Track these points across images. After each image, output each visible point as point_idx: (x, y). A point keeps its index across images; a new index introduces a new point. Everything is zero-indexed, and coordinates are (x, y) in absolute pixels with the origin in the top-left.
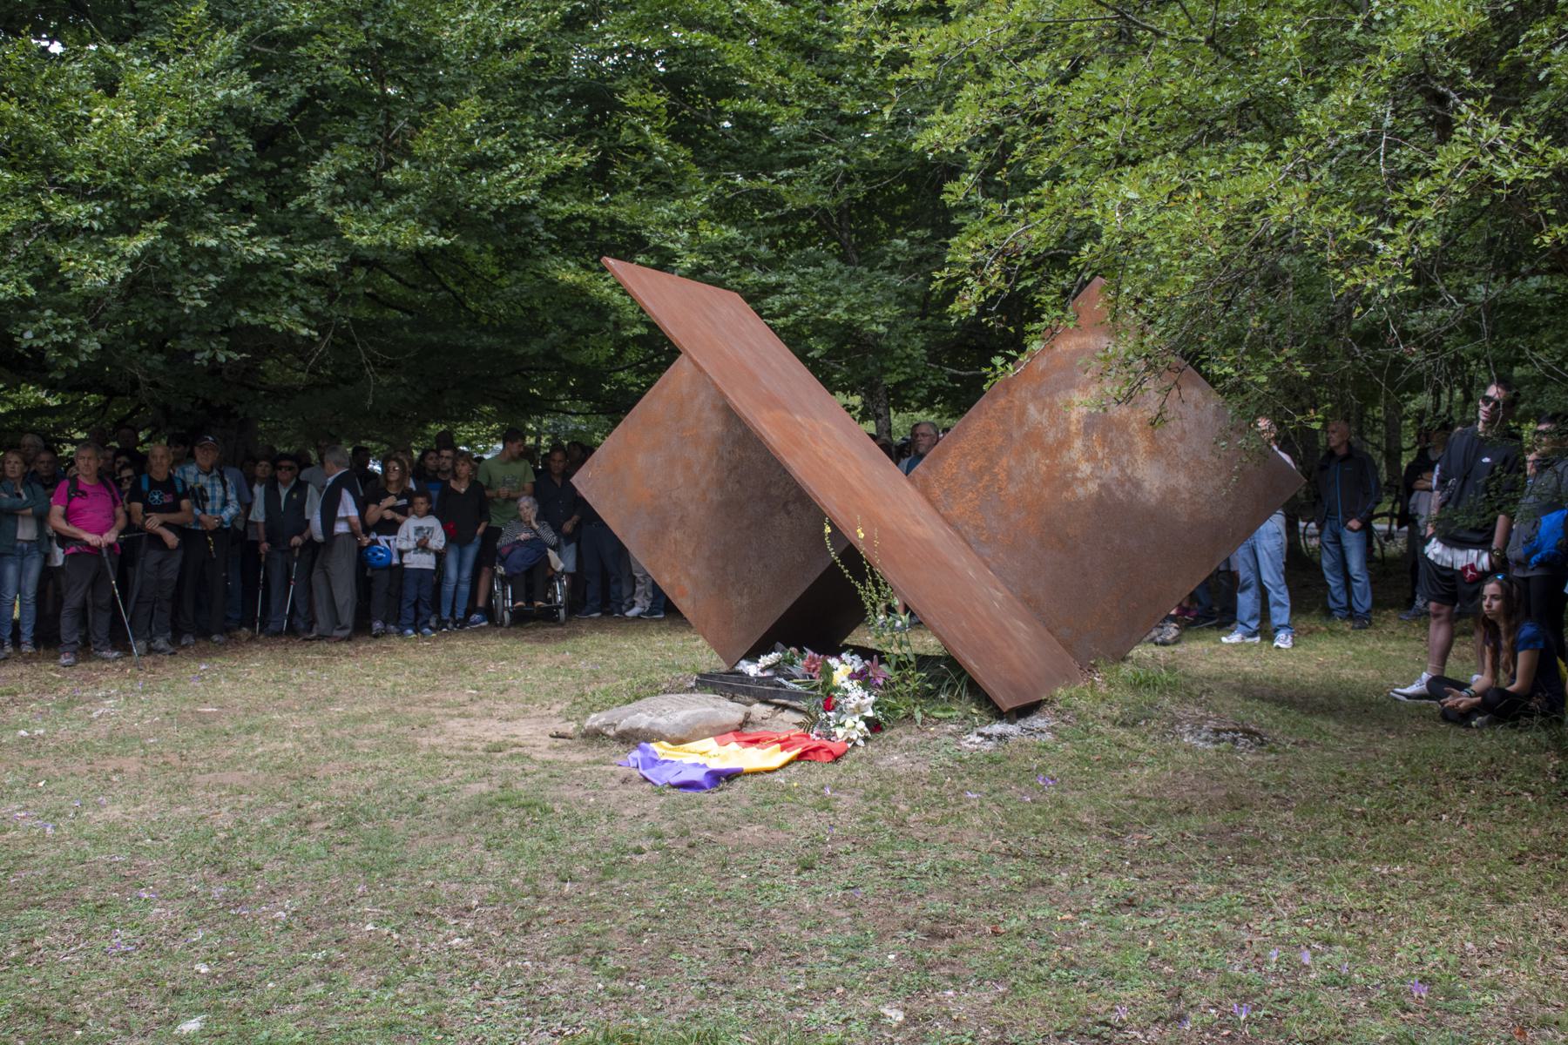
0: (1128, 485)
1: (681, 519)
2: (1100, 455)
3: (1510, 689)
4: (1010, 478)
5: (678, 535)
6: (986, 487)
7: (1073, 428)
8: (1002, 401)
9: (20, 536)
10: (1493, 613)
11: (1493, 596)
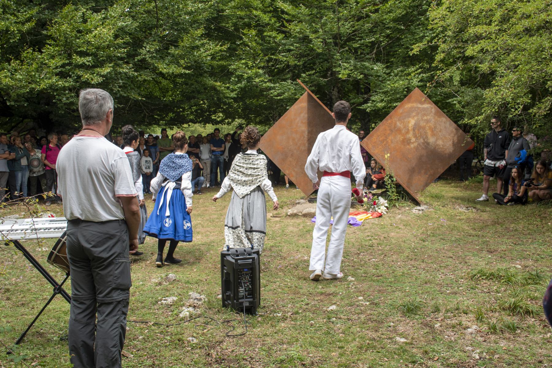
0: (425, 144)
1: (292, 155)
2: (418, 136)
3: (518, 195)
4: (392, 142)
5: (291, 159)
6: (385, 145)
7: (410, 129)
8: (389, 121)
9: (22, 164)
10: (515, 177)
11: (515, 172)
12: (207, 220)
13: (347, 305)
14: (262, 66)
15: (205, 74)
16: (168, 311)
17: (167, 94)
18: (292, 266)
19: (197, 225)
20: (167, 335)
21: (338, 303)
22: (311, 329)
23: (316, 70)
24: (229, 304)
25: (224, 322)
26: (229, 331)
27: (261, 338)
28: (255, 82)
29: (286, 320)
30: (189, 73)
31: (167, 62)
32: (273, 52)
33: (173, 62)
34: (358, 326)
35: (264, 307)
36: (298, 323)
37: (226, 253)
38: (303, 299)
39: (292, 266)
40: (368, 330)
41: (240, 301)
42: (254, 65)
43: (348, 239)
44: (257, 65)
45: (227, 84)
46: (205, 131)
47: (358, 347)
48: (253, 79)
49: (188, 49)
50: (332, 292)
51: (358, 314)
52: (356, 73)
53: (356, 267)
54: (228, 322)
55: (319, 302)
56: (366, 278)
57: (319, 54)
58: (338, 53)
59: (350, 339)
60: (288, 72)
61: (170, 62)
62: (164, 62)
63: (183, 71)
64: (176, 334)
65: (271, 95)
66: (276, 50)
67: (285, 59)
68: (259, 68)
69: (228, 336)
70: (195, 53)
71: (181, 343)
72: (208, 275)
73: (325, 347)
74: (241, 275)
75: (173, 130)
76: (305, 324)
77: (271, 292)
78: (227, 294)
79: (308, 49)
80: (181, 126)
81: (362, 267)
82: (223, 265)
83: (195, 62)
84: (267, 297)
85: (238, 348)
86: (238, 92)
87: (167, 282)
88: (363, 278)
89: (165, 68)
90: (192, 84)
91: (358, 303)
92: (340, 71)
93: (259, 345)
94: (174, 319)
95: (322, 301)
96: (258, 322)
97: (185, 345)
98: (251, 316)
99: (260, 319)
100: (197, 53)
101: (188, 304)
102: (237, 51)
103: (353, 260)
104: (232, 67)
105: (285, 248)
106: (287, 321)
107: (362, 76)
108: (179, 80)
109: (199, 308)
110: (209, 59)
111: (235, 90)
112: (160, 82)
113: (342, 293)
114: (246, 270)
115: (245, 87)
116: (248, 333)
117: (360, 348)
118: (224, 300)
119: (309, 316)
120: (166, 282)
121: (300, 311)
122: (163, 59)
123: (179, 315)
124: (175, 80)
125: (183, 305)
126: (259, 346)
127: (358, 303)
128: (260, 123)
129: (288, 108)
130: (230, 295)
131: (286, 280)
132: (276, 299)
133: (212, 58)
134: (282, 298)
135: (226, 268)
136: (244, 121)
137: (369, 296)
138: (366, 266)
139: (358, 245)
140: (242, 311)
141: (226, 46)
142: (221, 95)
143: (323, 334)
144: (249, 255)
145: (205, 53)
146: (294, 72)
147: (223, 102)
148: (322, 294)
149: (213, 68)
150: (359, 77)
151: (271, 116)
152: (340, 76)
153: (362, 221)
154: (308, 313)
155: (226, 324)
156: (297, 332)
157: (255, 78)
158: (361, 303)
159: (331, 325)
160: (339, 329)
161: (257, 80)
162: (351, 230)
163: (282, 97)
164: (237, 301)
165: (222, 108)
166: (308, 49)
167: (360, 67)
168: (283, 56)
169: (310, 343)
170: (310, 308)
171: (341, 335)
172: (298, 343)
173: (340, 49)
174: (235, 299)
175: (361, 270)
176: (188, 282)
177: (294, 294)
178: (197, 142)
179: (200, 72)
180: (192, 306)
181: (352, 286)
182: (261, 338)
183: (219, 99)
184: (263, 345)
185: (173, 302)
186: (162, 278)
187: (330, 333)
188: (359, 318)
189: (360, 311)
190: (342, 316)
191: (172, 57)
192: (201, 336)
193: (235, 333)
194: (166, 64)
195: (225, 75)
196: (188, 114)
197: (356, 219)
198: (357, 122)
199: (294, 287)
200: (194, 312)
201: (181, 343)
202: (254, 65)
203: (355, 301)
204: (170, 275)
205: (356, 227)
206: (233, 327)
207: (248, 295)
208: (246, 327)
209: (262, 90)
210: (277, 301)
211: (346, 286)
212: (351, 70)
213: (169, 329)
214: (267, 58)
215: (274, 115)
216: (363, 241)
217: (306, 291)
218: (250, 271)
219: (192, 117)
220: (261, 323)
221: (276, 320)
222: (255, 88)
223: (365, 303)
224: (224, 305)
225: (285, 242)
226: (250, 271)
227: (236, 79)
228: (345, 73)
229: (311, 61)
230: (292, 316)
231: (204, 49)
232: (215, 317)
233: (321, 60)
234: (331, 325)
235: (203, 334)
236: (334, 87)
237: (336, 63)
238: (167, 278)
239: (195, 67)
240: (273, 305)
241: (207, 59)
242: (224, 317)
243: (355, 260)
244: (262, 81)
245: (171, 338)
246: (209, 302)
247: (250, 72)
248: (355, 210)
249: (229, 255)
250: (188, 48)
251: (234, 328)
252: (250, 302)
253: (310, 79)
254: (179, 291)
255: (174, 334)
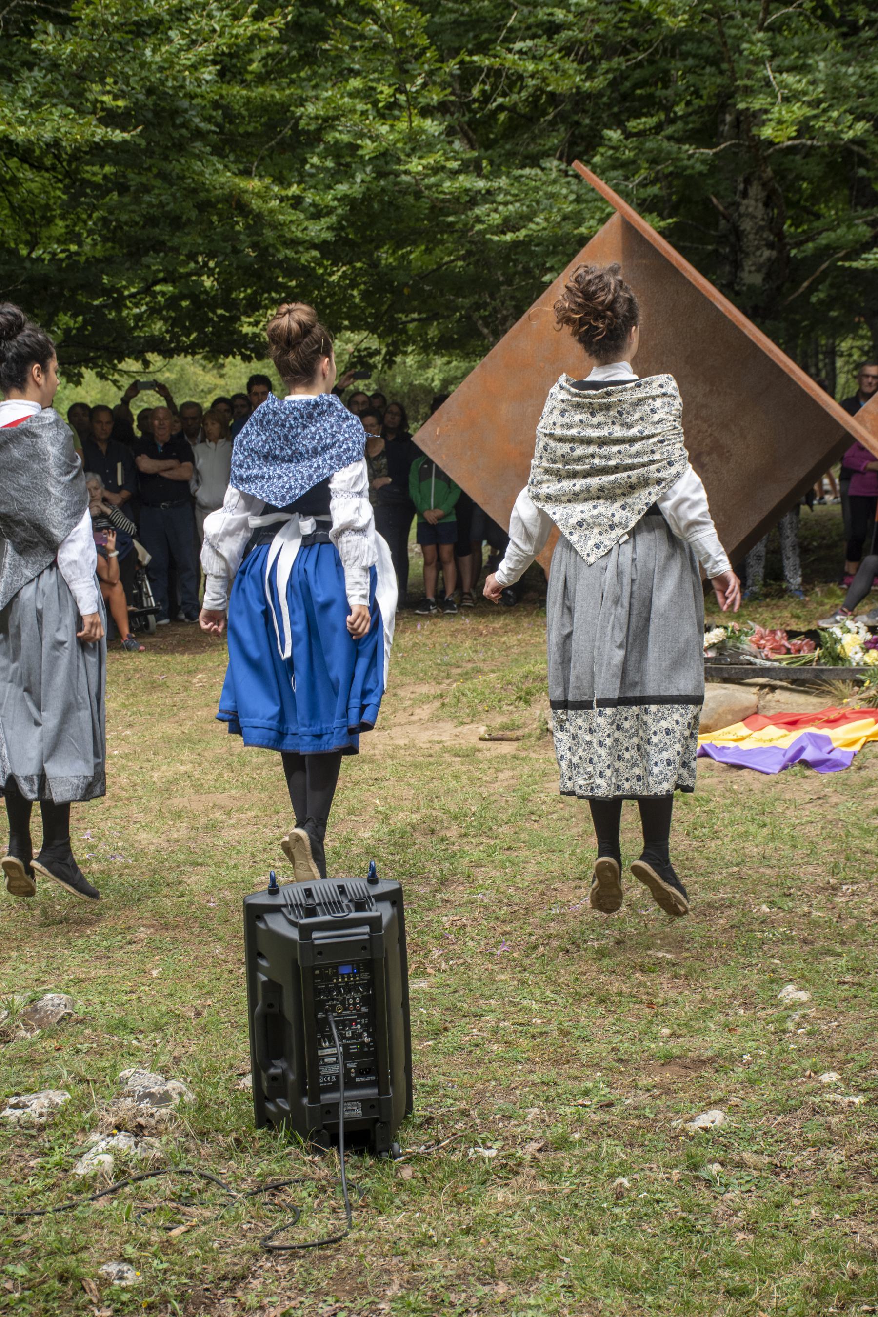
12: (218, 760)
13: (772, 1107)
14: (434, 102)
15: (198, 146)
16: (27, 1152)
17: (45, 233)
18: (555, 943)
19: (175, 781)
20: (20, 1258)
21: (734, 1100)
22: (617, 1210)
23: (668, 109)
24: (282, 1113)
25: (260, 1191)
26: (277, 1231)
27: (404, 1253)
28: (406, 172)
29: (517, 1173)
30: (125, 141)
31: (29, 93)
32: (485, 36)
33: (54, 95)
34: (812, 1198)
35: (429, 1120)
36: (566, 1187)
37: (265, 900)
38: (590, 1085)
39: (555, 943)
40: (854, 1213)
41: (327, 1098)
42: (402, 98)
43: (794, 827)
44: (412, 100)
45: (290, 185)
46: (222, 382)
47: (808, 1288)
48: (399, 161)
49: (116, 36)
50: (710, 1053)
51: (818, 1145)
52: (835, 114)
53: (818, 945)
54: (277, 1188)
55: (654, 1097)
56: (860, 992)
57: (678, 39)
58: (761, 28)
59: (778, 1253)
60: (552, 123)
61: (44, 95)
62: (14, 91)
63: (100, 133)
64: (52, 1253)
65: (479, 227)
66: (499, 29)
67: (531, 67)
68: (426, 112)
69: (270, 1250)
70: (148, 52)
71: (69, 1290)
72: (209, 993)
73: (672, 1288)
74: (329, 991)
75: (78, 383)
76: (592, 1190)
77: (459, 1059)
78: (272, 1071)
79: (628, 17)
80: (114, 368)
81: (843, 943)
82: (254, 954)
83: (150, 92)
84: (442, 1079)
85: (308, 1302)
86: (342, 218)
87: (32, 1030)
88: (844, 992)
89: (22, 123)
90: (147, 189)
91: (817, 1100)
92: (766, 111)
93: (395, 1287)
94: (50, 1188)
95: (668, 1092)
96: (400, 1184)
97: (87, 1297)
98: (369, 1161)
99: (407, 1173)
100: (154, 51)
101: (113, 1120)
102: (326, 38)
103: (807, 915)
104: (311, 109)
105: (532, 867)
106: (520, 1179)
107: (861, 127)
108: (95, 173)
109: (158, 1135)
110: (207, 77)
111: (330, 211)
112: (15, 182)
113: (755, 1056)
114: (345, 970)
115: (368, 197)
116: (353, 1235)
117: (817, 1295)
118: (261, 1097)
119: (613, 1154)
120: (31, 1030)
121: (577, 1136)
122: (10, 80)
123: (72, 1166)
124: (77, 171)
125: (93, 1125)
126: (393, 1290)
127: (817, 1100)
128: (445, 345)
129: (546, 278)
130: (284, 1075)
131: (525, 1003)
132: (479, 1086)
133: (221, 74)
134: (505, 1083)
135: (264, 963)
136: (374, 343)
137: (862, 1069)
138: (860, 938)
139: (832, 853)
140: (334, 1141)
141: (278, 19)
142: (269, 233)
143: (664, 1231)
144: (360, 907)
145: (188, 50)
146: (577, 124)
147: (280, 263)
148: (669, 1060)
149: (229, 115)
150: (851, 134)
151: (484, 318)
152: (767, 132)
153: (857, 748)
154: (607, 1145)
155: (265, 1197)
156: (558, 1225)
157: (408, 155)
158: (829, 1097)
159: (704, 1196)
160: (735, 1213)
161: (416, 165)
162: (807, 787)
163: (522, 234)
164: (315, 1099)
165: (284, 287)
166: (628, 17)
167: (855, 86)
168: (520, 52)
169: (606, 1273)
170: (616, 1120)
171: (741, 1236)
172: (557, 1272)
173: (767, 12)
174: (304, 1093)
175: (840, 955)
176: (122, 1025)
177: (556, 1063)
178: (180, 435)
179: (175, 134)
180: (130, 1125)
181: (799, 1025)
182: (404, 1253)
183: (263, 251)
184: (412, 1285)
185: (51, 1114)
186: (12, 1012)
187: (692, 1230)
188: (820, 1163)
189: (825, 1135)
190: (746, 1155)
191: (49, 71)
192: (155, 1256)
193: (300, 1236)
194: (24, 101)
195: (283, 146)
196: (138, 318)
197: (828, 741)
198: (858, 326)
199: (555, 1034)
200: (138, 1153)
201: (69, 1290)
202: (402, 98)
203: (802, 1089)
204: (49, 996)
205: (827, 776)
206: (294, 1209)
207: (361, 1072)
208: (349, 1207)
209: (438, 209)
210: (481, 1094)
211: (771, 1028)
212: (817, 103)
213: (25, 1231)
214: (452, 66)
215: (495, 311)
216: (856, 833)
217: (603, 1048)
218: (365, 976)
219: (158, 327)
220: (411, 1192)
221: (475, 1177)
222: (411, 199)
223: (847, 1100)
224: (264, 1120)
225: (530, 845)
226: (365, 976)
227: (330, 164)
228: (786, 116)
229: (647, 71)
230: (541, 1156)
231: (184, 36)
232: (225, 1170)
233: (690, 62)
234: (704, 1196)
235: (167, 1245)
236: (747, 181)
237: (749, 75)
238: (35, 1010)
239: (150, 115)
240: (465, 1113)
241: (198, 79)
242: (258, 1171)
243: (816, 914)
244: (437, 169)
245: (32, 1270)
246: (201, 1107)
247: (384, 129)
248: (827, 701)
249: (276, 909)
250: (117, 28)
251: (297, 1213)
252: (368, 1104)
253: (640, 150)
254: (80, 1065)
255: (43, 1253)
